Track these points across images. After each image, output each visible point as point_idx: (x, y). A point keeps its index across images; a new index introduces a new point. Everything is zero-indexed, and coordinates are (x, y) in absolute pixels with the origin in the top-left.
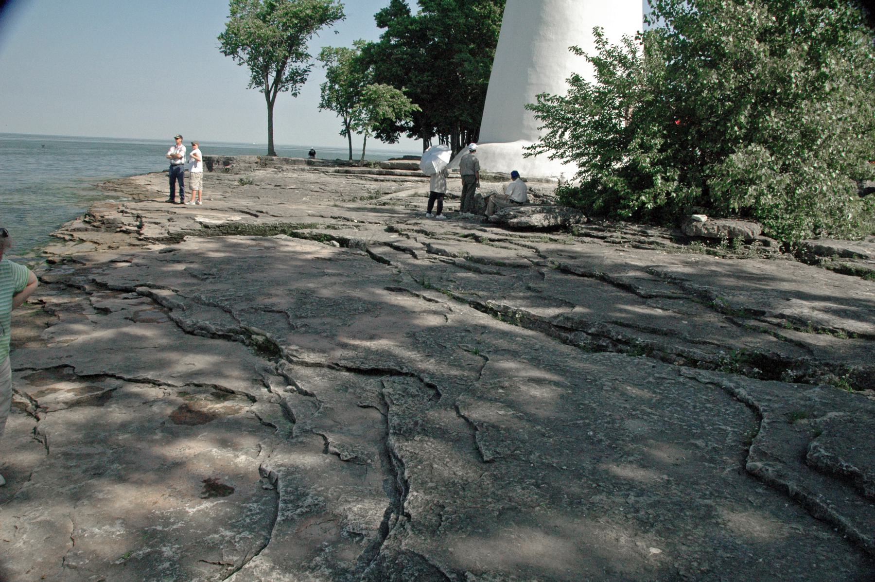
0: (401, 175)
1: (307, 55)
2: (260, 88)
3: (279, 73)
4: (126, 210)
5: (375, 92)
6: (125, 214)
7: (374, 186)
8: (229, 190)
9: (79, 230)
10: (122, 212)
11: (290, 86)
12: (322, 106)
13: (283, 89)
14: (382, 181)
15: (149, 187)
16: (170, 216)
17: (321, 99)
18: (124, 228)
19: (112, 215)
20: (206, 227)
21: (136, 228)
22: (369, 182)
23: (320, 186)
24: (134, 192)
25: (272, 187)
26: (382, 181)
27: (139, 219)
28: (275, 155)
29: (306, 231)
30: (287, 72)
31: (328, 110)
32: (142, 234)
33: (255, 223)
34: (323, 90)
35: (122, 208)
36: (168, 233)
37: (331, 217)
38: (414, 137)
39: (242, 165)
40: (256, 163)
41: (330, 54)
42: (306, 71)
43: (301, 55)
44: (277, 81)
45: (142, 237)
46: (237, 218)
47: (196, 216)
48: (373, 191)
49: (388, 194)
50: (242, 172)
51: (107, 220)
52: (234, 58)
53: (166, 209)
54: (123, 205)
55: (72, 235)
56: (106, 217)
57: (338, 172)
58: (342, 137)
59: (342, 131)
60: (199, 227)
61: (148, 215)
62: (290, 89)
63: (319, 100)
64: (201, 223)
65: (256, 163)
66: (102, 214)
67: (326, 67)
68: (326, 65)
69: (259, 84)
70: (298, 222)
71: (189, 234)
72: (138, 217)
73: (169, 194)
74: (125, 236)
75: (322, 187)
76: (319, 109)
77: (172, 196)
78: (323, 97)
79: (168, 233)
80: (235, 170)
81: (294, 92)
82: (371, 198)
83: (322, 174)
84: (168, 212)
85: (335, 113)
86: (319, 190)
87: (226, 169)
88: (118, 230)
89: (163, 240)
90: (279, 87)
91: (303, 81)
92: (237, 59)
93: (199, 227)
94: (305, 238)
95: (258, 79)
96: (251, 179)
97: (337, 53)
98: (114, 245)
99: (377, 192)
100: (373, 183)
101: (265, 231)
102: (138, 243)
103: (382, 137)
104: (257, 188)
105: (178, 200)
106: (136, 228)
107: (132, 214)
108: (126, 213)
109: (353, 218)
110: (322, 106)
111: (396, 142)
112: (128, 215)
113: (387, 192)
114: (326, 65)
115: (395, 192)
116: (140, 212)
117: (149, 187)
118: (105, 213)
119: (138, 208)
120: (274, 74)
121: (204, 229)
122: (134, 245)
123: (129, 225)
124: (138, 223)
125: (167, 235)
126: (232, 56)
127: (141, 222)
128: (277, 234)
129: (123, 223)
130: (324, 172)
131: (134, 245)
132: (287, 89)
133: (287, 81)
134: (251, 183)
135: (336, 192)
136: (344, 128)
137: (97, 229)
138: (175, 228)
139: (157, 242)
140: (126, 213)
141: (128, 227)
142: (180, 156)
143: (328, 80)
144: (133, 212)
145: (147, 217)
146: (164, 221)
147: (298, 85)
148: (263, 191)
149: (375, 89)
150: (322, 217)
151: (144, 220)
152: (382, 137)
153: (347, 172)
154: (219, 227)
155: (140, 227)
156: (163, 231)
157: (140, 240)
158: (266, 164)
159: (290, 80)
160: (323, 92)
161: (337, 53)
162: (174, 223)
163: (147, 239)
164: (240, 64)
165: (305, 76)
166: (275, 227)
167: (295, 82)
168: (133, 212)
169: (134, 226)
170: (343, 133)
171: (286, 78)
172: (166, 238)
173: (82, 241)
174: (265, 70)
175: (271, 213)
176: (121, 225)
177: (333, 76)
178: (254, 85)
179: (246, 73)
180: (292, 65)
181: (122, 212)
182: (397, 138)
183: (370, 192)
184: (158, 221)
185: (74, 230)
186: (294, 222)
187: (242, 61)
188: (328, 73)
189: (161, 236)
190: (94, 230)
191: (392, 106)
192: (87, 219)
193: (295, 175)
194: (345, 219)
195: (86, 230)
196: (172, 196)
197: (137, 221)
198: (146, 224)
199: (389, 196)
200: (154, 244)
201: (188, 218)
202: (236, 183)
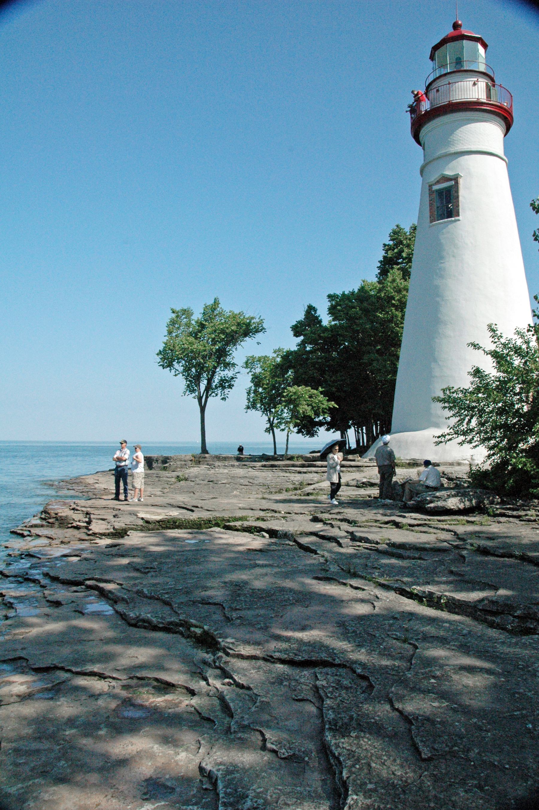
0: (322, 467)
1: (234, 365)
2: (193, 395)
3: (210, 381)
4: (78, 508)
5: (295, 393)
6: (76, 512)
7: (297, 478)
8: (167, 486)
9: (36, 526)
10: (73, 509)
11: (219, 391)
12: (248, 408)
13: (213, 394)
14: (305, 473)
15: (97, 486)
16: (115, 513)
17: (247, 401)
18: (74, 524)
19: (65, 512)
20: (147, 522)
21: (85, 524)
22: (293, 475)
23: (248, 480)
24: (84, 490)
25: (206, 482)
26: (305, 473)
27: (88, 516)
28: (208, 453)
29: (238, 524)
30: (216, 380)
31: (254, 410)
32: (91, 530)
33: (191, 518)
34: (249, 393)
35: (74, 506)
36: (114, 528)
37: (260, 510)
38: (332, 430)
39: (179, 463)
40: (191, 461)
41: (254, 362)
42: (233, 378)
43: (228, 364)
44: (208, 388)
45: (91, 532)
46: (175, 513)
47: (138, 512)
48: (297, 483)
49: (311, 484)
50: (179, 469)
51: (61, 517)
52: (171, 370)
53: (112, 506)
54: (74, 503)
55: (30, 531)
56: (60, 514)
57: (264, 466)
58: (267, 434)
59: (267, 429)
60: (141, 522)
61: (96, 512)
62: (219, 394)
63: (246, 403)
64: (142, 519)
65: (191, 461)
66: (56, 512)
67: (250, 374)
68: (250, 372)
69: (193, 391)
70: (230, 516)
71: (132, 529)
72: (87, 514)
73: (114, 491)
74: (76, 532)
75: (251, 481)
76: (245, 410)
77: (117, 494)
78: (248, 399)
79: (114, 528)
80: (172, 468)
81: (223, 396)
82: (296, 489)
83: (250, 469)
84: (114, 509)
85: (260, 413)
86: (248, 484)
87: (164, 467)
88: (70, 525)
89: (109, 535)
90: (210, 393)
91: (230, 386)
92: (173, 371)
93: (141, 522)
94: (237, 530)
95: (190, 389)
96: (187, 476)
97: (259, 361)
98: (66, 540)
99: (301, 484)
100: (297, 475)
101: (200, 525)
102: (87, 538)
103: (303, 432)
104: (192, 484)
105: (122, 497)
106: (85, 524)
107: (82, 511)
108: (77, 510)
109: (280, 509)
110: (248, 408)
111: (316, 436)
112: (78, 512)
113: (310, 482)
114: (250, 372)
115: (318, 482)
116: (89, 509)
117: (97, 486)
118: (59, 511)
119: (87, 506)
120: (205, 382)
121: (145, 524)
122: (83, 540)
123: (79, 521)
124: (87, 520)
125: (112, 530)
126: (169, 368)
127: (90, 518)
128: (211, 527)
129: (74, 520)
130: (252, 467)
131: (83, 540)
132: (217, 395)
133: (216, 387)
134: (186, 479)
135: (264, 485)
136: (268, 426)
137: (52, 525)
138: (119, 524)
139: (103, 537)
140: (77, 510)
141: (78, 523)
142: (124, 459)
143: (252, 384)
144: (83, 509)
145: (96, 514)
146: (110, 518)
147: (226, 391)
148: (197, 486)
149: (294, 391)
150: (252, 509)
151: (92, 516)
152: (303, 432)
153: (273, 466)
154: (159, 522)
155: (89, 523)
156: (109, 527)
157: (89, 535)
158: (200, 462)
159: (219, 387)
160: (248, 395)
161: (259, 361)
162: (119, 519)
163: (94, 534)
164: (176, 375)
165: (232, 383)
166: (210, 521)
167: (224, 388)
168: (83, 509)
169: (84, 522)
170: (267, 430)
171: (216, 385)
172: (112, 533)
173: (38, 536)
174: (197, 379)
175: (206, 508)
176: (72, 521)
177: (257, 381)
178: (188, 393)
179: (181, 382)
180: (221, 374)
181: (73, 509)
182: (316, 432)
183: (294, 484)
184: (105, 518)
185: (32, 526)
186: (226, 515)
187: (177, 372)
188: (252, 379)
189: (108, 531)
190: (47, 526)
191: (311, 405)
192: (43, 516)
193: (226, 471)
194: (273, 510)
195: (42, 526)
196: (117, 494)
197: (86, 517)
198: (94, 521)
199: (312, 487)
200: (101, 539)
201: (131, 514)
202: (173, 480)
